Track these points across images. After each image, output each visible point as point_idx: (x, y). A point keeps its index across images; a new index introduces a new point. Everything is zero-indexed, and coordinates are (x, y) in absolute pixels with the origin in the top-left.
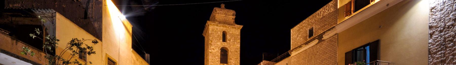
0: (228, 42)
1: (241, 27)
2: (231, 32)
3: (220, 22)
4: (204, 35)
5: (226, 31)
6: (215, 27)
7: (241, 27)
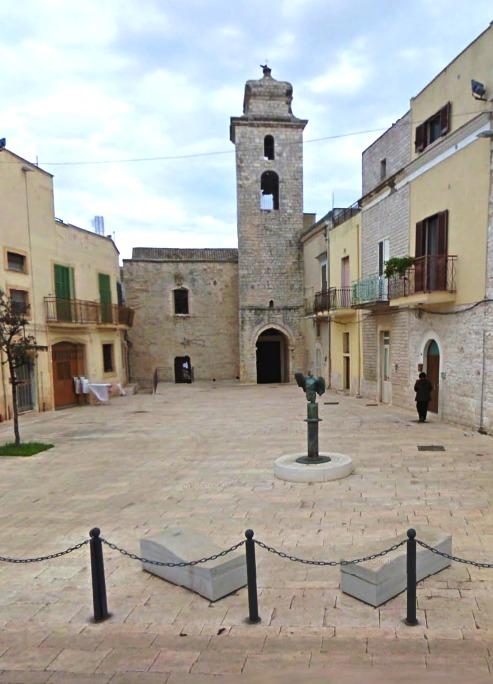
5: (272, 134)
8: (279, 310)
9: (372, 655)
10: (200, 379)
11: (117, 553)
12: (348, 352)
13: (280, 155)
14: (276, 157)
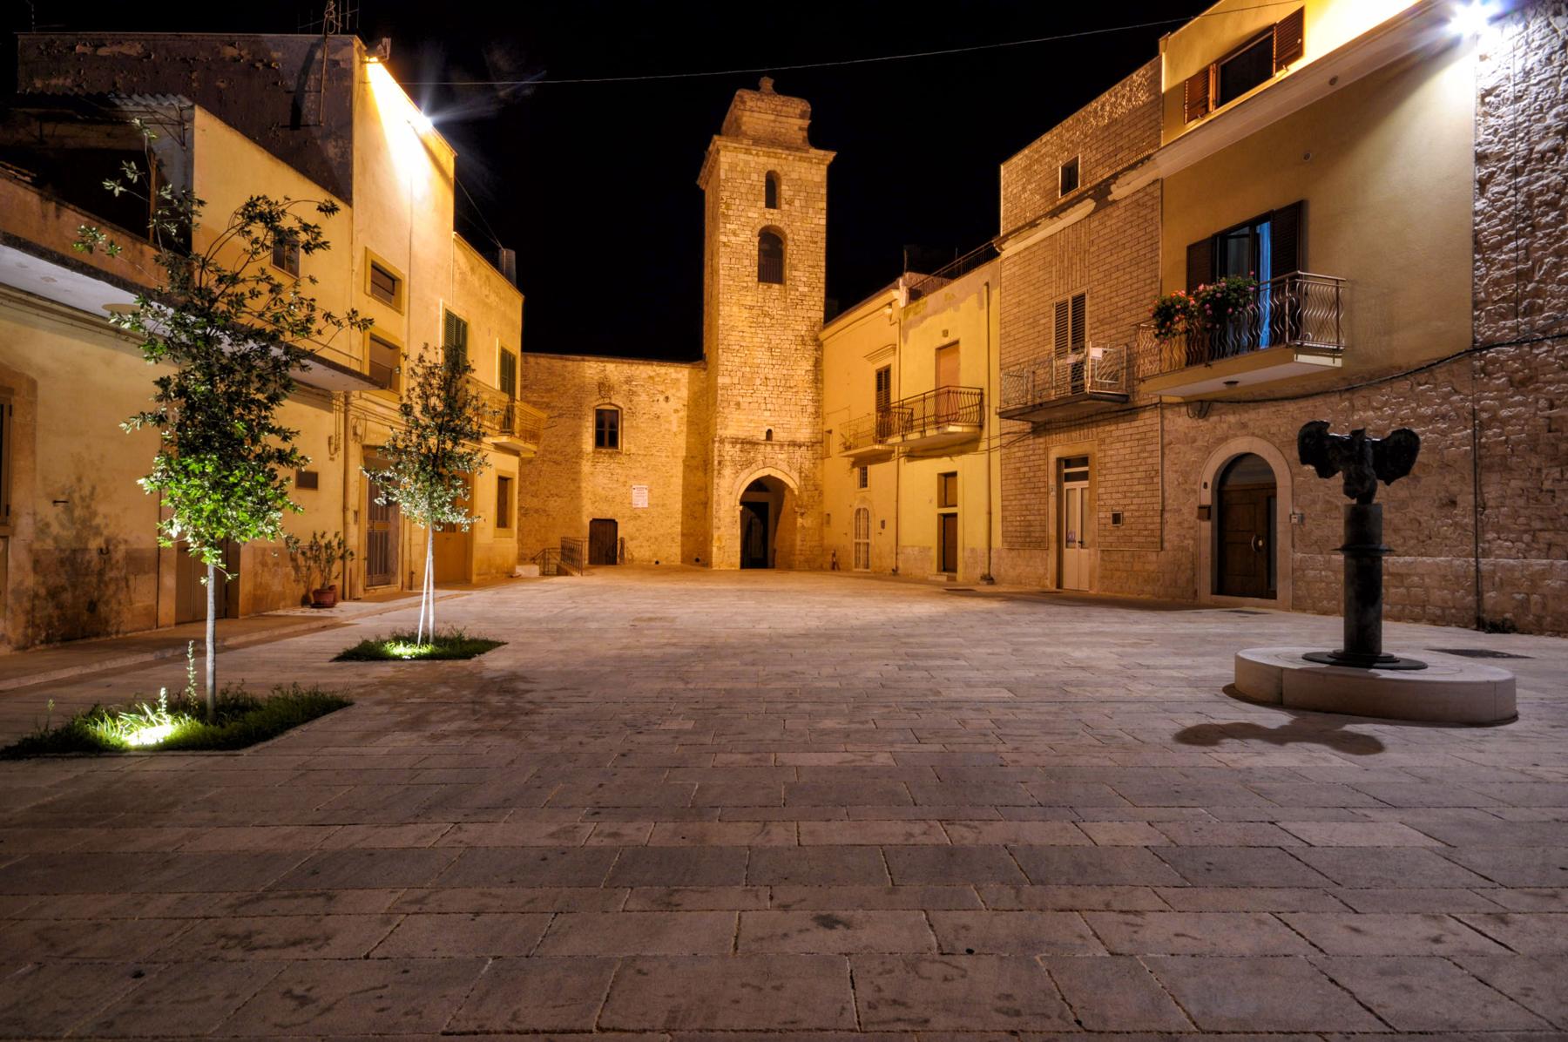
3: (757, 141)
4: (701, 183)
5: (778, 169)
12: (945, 516)
13: (790, 203)
14: (785, 207)
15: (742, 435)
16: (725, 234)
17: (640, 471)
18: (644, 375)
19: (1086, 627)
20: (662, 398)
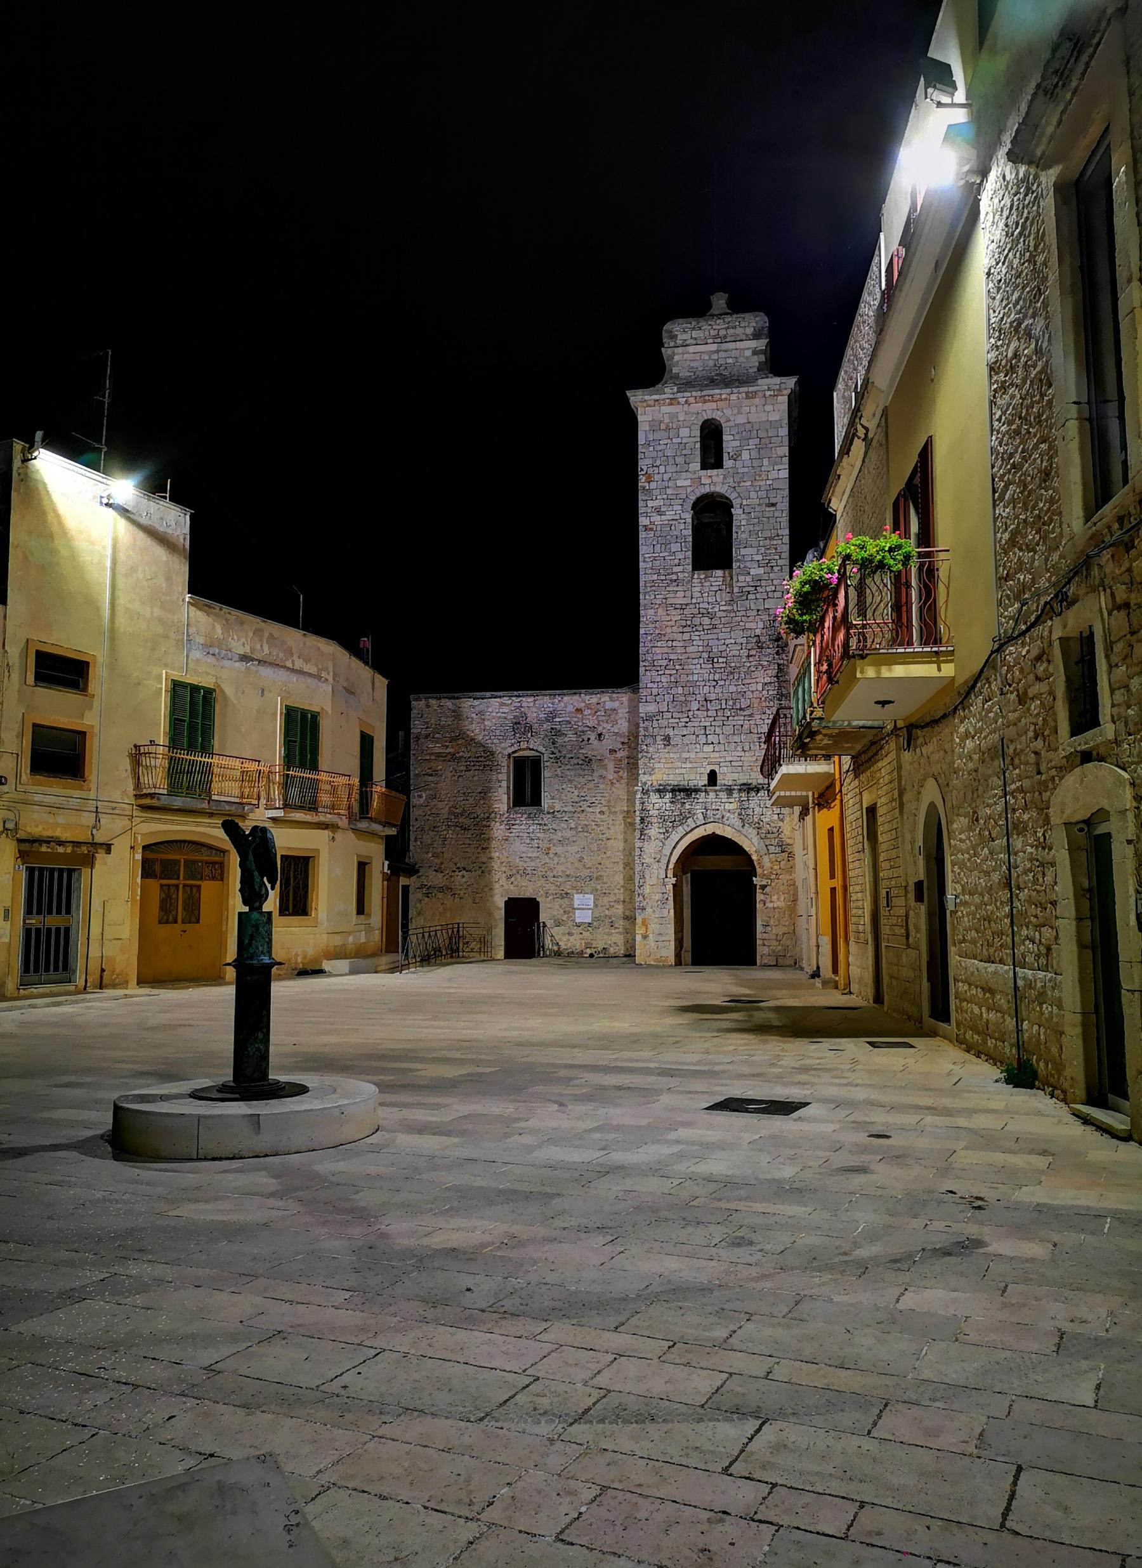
0: (727, 463)
1: (791, 382)
2: (741, 419)
3: (687, 385)
4: (176, 520)
5: (717, 415)
6: (665, 409)
7: (790, 382)
8: (729, 791)
9: (988, 1009)
10: (558, 954)
11: (719, 1383)
15: (673, 780)
16: (646, 515)
17: (568, 834)
18: (570, 708)
19: (332, 1039)
20: (593, 736)
